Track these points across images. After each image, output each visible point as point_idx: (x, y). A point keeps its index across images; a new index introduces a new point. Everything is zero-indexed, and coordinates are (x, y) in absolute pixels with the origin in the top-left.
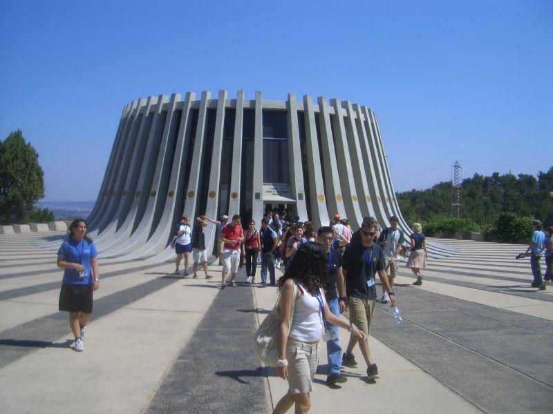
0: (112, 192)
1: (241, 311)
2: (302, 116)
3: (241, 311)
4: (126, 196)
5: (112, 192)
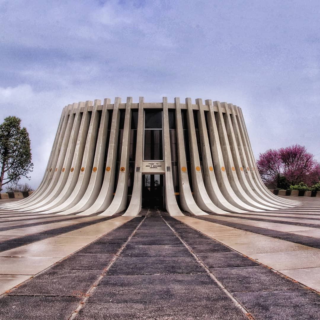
5: (55, 169)
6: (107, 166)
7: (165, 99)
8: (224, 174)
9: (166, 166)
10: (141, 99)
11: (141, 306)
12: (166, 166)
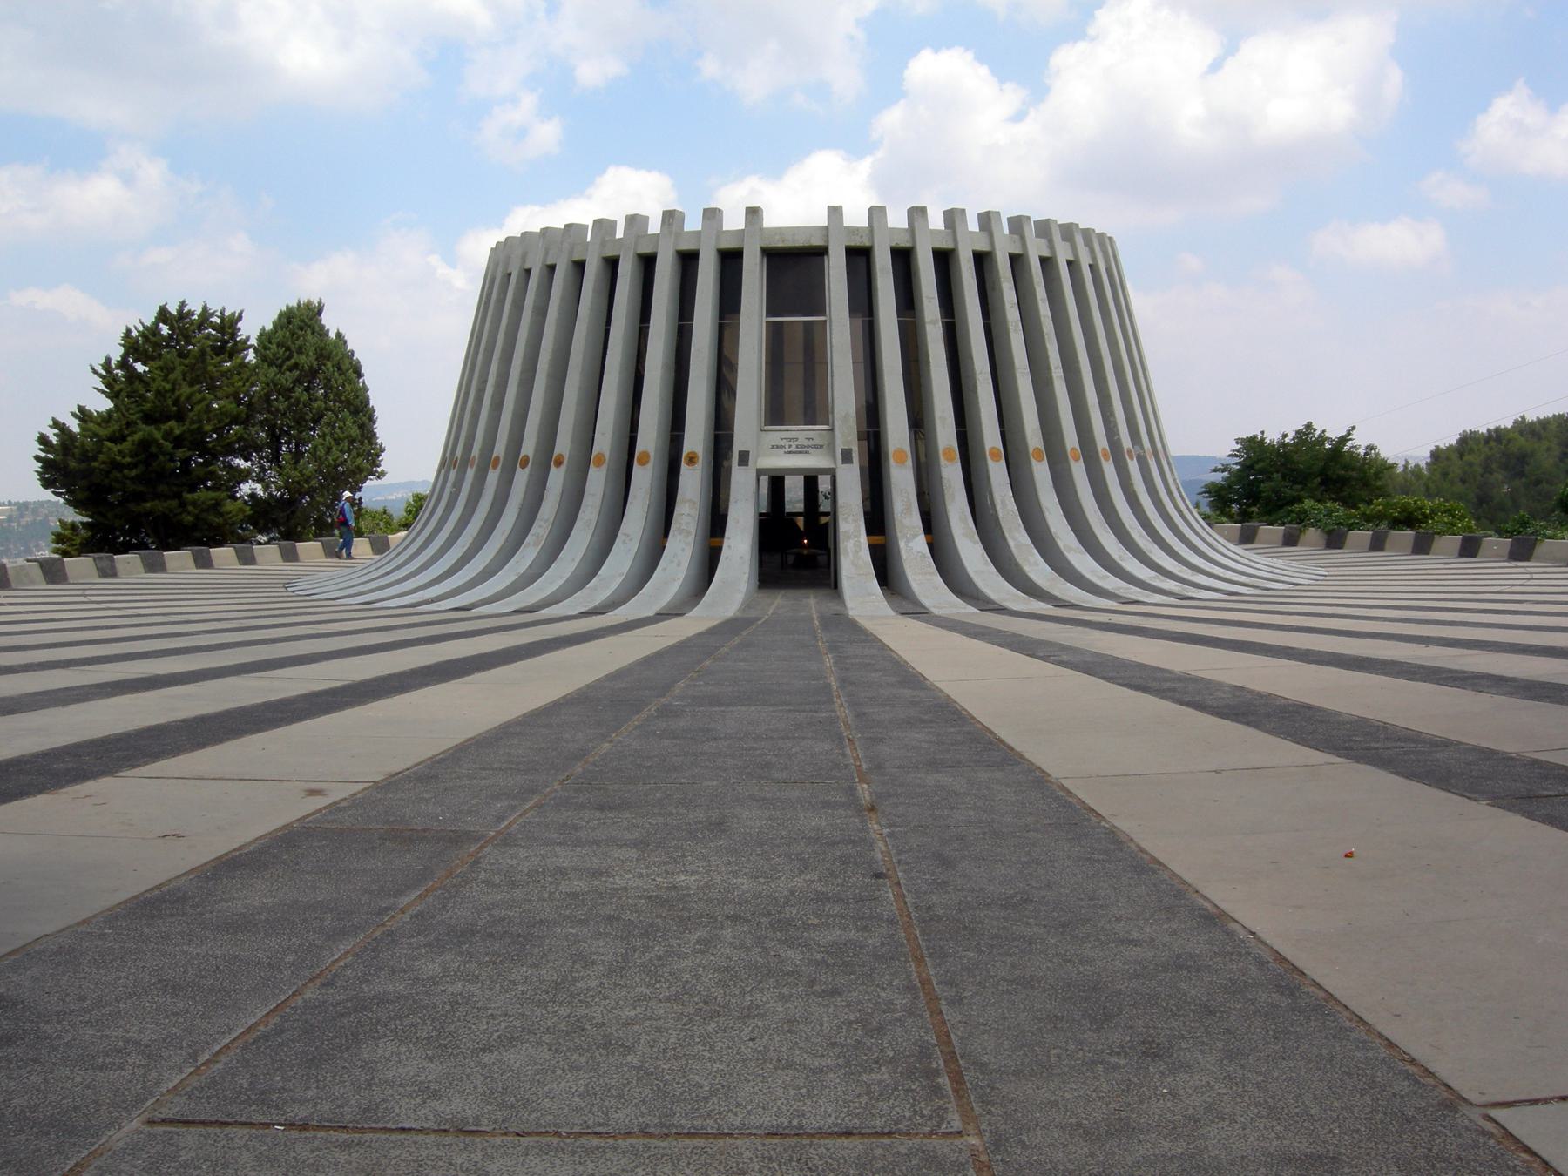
0: (466, 461)
1: (164, 1121)
2: (1016, 260)
3: (164, 1121)
4: (527, 470)
5: (514, 458)
6: (639, 449)
7: (835, 212)
8: (1041, 471)
9: (840, 445)
10: (753, 213)
11: (633, 854)
12: (840, 445)
